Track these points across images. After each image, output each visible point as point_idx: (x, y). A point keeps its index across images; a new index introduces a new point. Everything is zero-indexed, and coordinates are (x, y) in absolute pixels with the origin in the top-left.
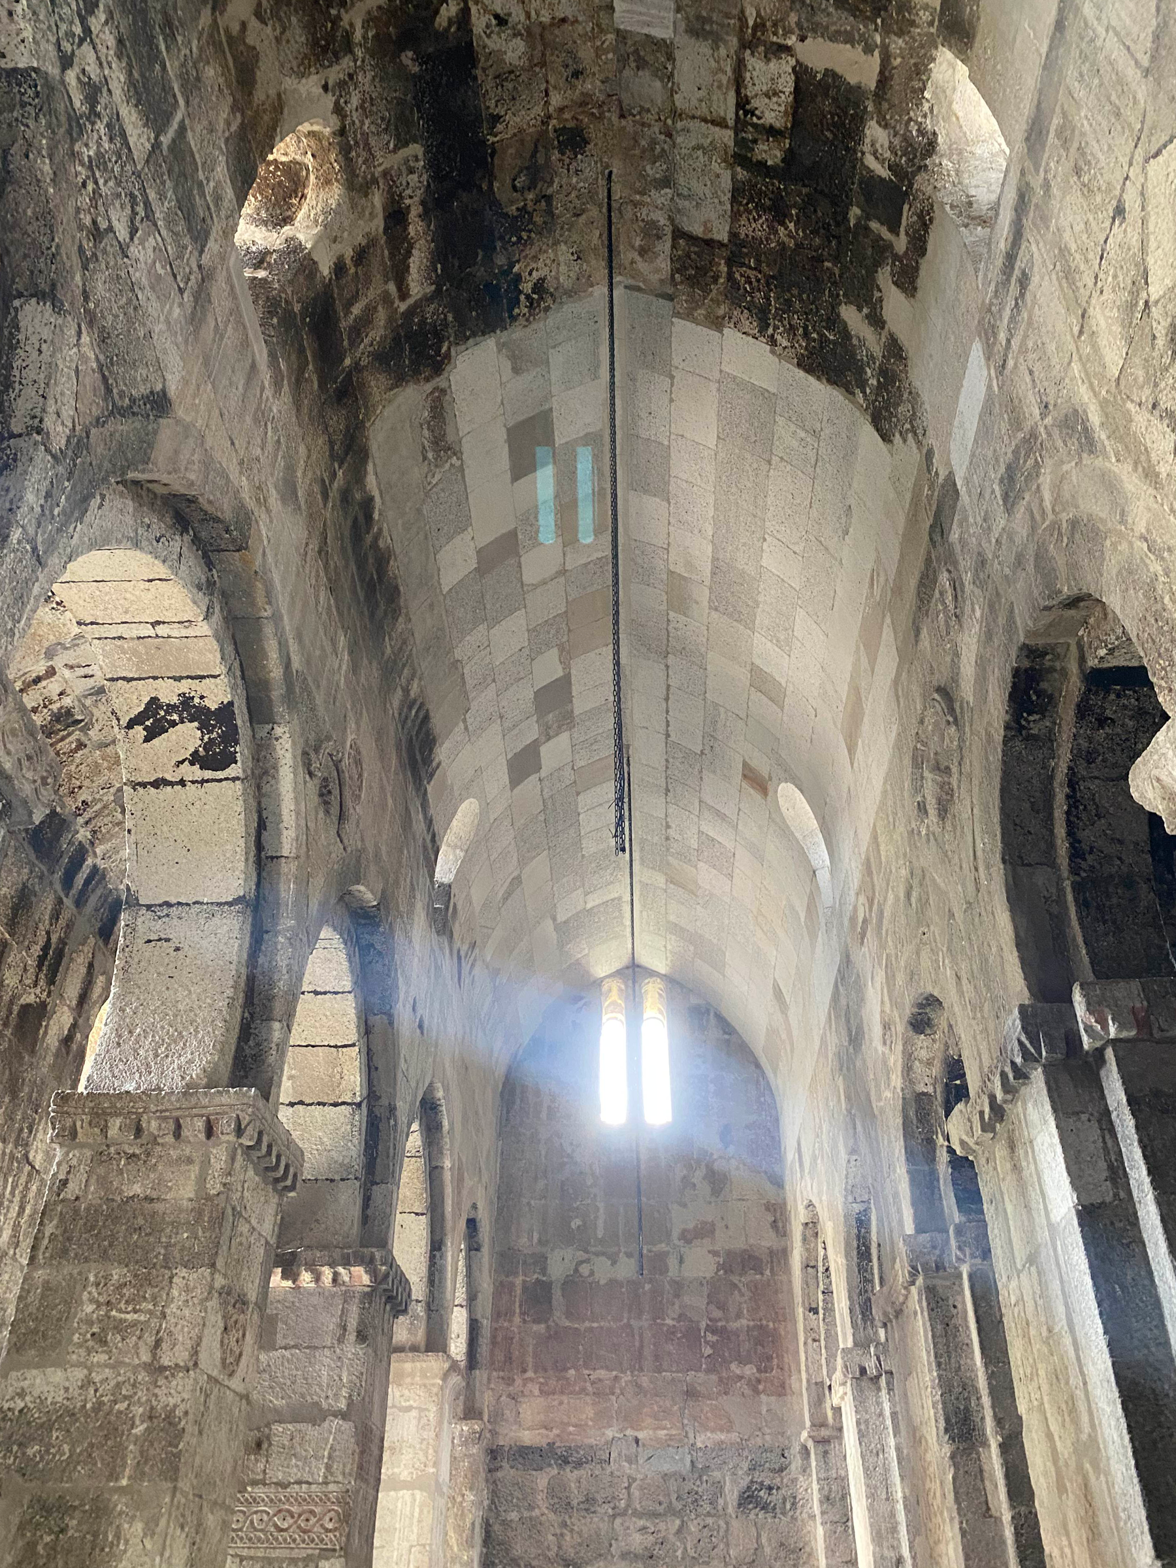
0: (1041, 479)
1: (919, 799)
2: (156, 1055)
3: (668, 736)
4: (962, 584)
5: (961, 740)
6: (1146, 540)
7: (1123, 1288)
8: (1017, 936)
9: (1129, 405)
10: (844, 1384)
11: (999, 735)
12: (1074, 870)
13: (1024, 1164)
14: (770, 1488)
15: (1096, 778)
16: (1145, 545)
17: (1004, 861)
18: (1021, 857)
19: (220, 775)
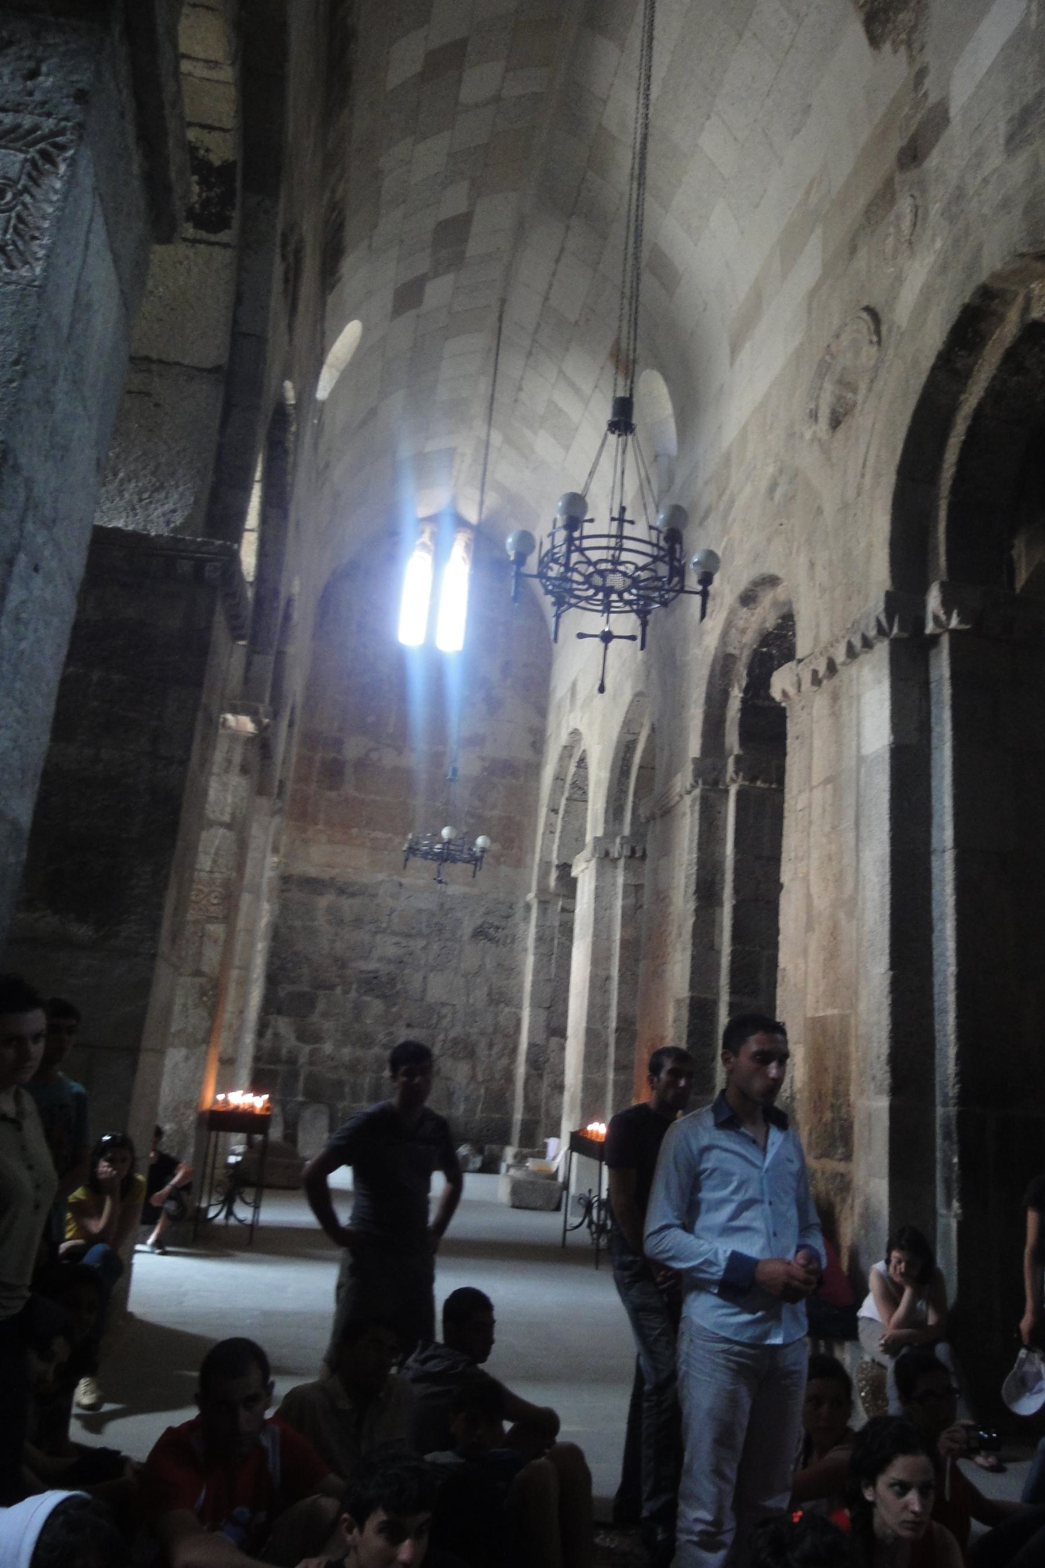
2: (141, 500)
3: (547, 299)
4: (927, 212)
5: (880, 360)
10: (588, 861)
11: (927, 362)
13: (845, 712)
14: (497, 928)
19: (213, 238)
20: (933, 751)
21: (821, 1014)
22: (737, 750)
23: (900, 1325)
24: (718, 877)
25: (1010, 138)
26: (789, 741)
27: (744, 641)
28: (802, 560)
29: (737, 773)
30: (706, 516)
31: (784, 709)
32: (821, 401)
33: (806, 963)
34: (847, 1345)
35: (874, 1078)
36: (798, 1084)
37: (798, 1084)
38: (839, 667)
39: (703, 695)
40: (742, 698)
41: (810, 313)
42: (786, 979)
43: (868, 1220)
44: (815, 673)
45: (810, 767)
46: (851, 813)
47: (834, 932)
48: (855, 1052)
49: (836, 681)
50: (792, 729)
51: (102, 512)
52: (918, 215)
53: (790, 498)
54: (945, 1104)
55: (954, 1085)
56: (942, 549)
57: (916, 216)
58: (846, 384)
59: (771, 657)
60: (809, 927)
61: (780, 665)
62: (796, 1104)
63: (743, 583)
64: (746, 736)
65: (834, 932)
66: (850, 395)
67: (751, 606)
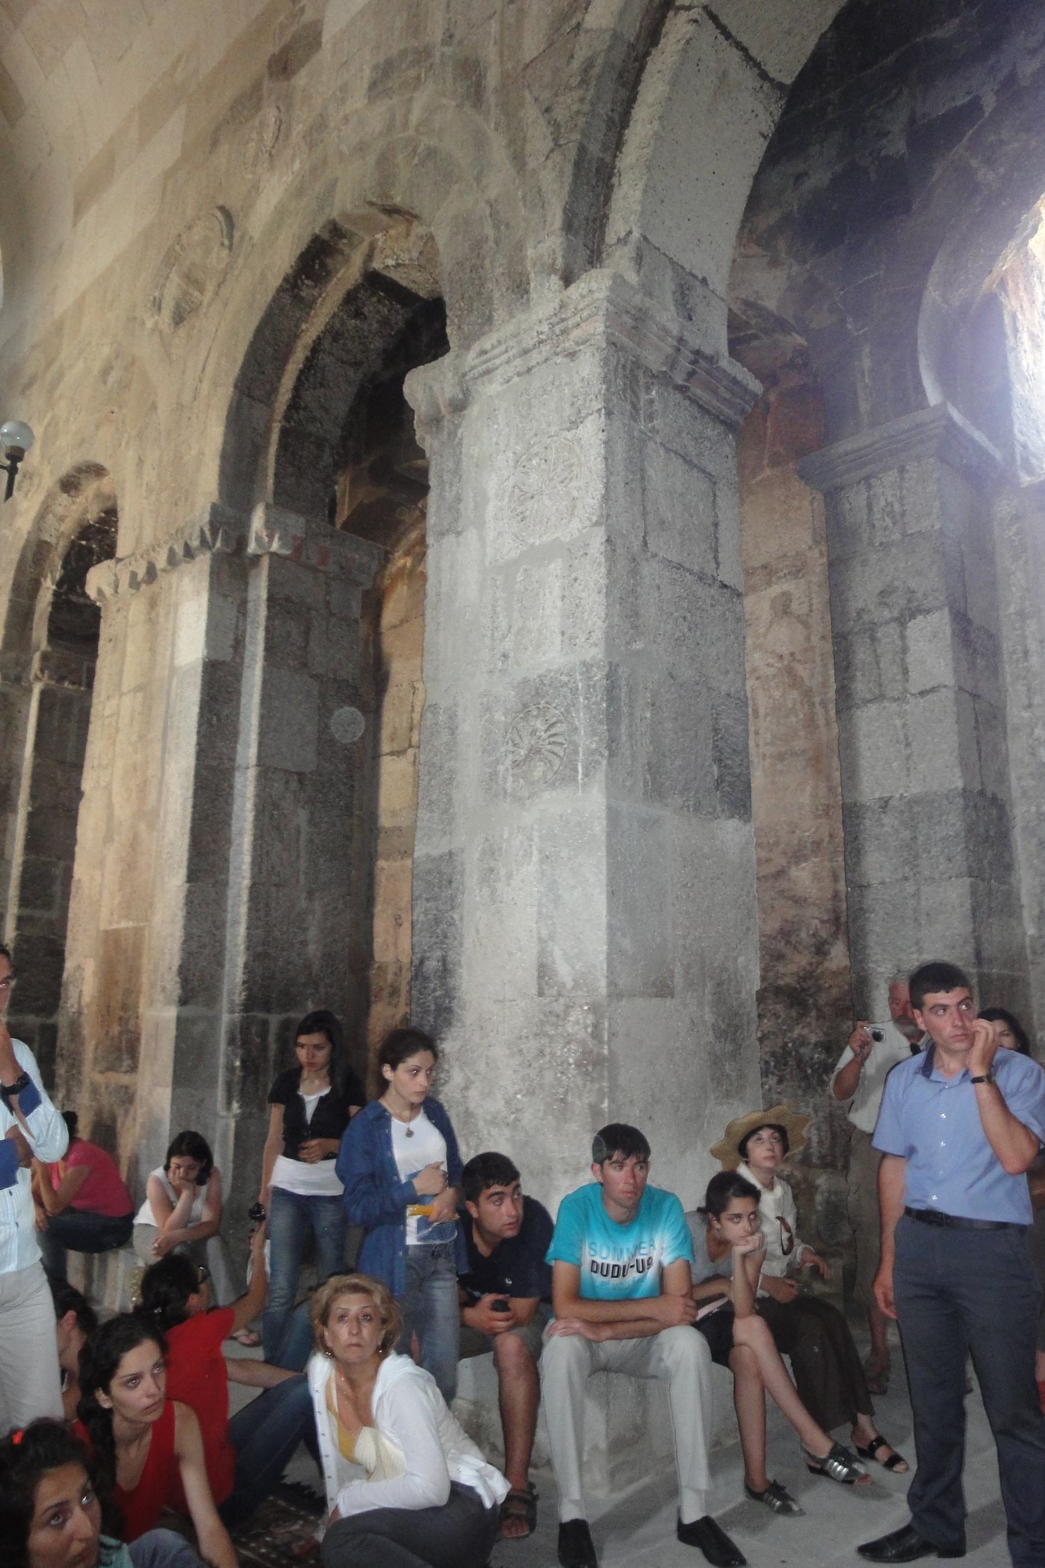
0: (417, 94)
1: (157, 294)
4: (289, 130)
5: (230, 266)
6: (491, 206)
7: (219, 719)
8: (224, 449)
9: (527, 93)
11: (275, 282)
12: (287, 417)
13: (162, 620)
15: (333, 355)
16: (488, 211)
17: (236, 387)
18: (249, 388)
20: (245, 669)
21: (114, 926)
22: (44, 646)
23: (172, 1228)
24: (14, 782)
25: (373, 85)
26: (101, 643)
27: (62, 529)
28: (130, 455)
29: (42, 670)
30: (29, 386)
31: (99, 609)
32: (166, 292)
33: (103, 875)
34: (122, 1253)
35: (164, 989)
36: (86, 999)
37: (86, 999)
38: (159, 573)
39: (11, 582)
40: (55, 591)
41: (164, 194)
42: (80, 891)
43: (151, 1131)
44: (134, 575)
45: (121, 673)
46: (159, 725)
47: (134, 844)
48: (146, 964)
49: (154, 587)
50: (105, 631)
51: (578, 112)
52: (282, 131)
53: (124, 386)
54: (232, 1012)
55: (240, 993)
56: (271, 472)
57: (279, 130)
58: (192, 280)
59: (91, 551)
60: (108, 839)
61: (99, 561)
62: (83, 1019)
63: (66, 466)
64: (55, 633)
65: (134, 844)
66: (196, 294)
67: (73, 493)
